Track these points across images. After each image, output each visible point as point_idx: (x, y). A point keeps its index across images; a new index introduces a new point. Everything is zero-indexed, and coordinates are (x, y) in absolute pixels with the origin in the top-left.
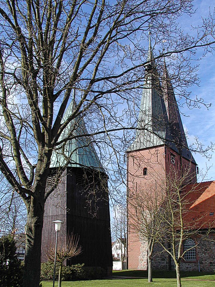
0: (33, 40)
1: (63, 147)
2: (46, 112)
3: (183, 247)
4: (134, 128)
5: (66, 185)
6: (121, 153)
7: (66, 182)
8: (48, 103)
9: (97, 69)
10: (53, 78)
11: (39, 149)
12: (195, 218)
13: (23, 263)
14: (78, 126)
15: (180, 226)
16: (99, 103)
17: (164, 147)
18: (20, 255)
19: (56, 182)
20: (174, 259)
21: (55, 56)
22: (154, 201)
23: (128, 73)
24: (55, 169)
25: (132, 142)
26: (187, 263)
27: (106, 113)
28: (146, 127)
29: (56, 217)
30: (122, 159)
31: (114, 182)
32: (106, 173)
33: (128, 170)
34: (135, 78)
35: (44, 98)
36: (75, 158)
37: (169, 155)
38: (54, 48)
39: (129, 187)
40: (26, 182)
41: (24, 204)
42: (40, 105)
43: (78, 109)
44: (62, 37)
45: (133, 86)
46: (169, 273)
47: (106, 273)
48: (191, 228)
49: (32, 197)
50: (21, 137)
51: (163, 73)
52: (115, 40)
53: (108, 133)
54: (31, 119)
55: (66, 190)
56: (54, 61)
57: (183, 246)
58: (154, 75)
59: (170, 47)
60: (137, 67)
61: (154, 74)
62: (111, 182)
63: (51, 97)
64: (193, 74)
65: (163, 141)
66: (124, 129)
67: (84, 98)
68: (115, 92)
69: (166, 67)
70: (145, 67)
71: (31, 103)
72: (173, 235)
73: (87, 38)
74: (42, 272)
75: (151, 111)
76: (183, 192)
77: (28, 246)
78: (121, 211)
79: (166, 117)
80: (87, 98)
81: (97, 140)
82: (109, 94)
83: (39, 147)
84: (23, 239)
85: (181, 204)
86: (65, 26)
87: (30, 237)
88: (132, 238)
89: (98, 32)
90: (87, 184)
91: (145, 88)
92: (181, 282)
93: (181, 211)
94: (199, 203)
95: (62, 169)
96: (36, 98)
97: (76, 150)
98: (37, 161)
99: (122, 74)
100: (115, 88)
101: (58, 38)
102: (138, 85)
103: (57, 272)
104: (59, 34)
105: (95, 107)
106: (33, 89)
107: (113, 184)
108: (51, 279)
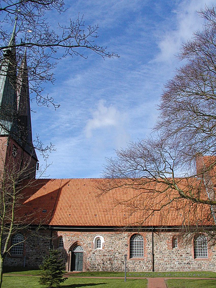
3: (11, 242)
12: (27, 214)
15: (11, 220)
26: (13, 258)
48: (21, 222)
57: (12, 241)
59: (33, 38)
64: (50, 72)
72: (2, 229)
85: (15, 198)
92: (3, 278)
93: (14, 205)
94: (34, 199)
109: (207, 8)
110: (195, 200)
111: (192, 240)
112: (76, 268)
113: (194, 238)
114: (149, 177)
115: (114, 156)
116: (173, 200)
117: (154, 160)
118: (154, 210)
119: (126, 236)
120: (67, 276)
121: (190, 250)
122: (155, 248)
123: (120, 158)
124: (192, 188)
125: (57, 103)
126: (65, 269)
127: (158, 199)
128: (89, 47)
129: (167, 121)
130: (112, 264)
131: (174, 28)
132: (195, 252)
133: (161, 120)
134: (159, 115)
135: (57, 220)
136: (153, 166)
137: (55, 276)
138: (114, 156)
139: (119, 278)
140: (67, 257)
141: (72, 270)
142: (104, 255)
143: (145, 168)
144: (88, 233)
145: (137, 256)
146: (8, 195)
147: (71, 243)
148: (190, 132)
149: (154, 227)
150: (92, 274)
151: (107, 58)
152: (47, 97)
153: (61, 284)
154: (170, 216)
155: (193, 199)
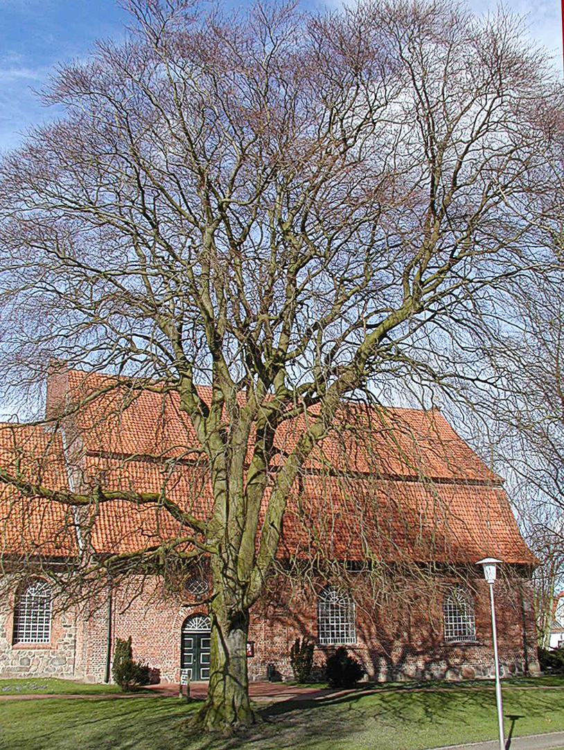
136: (224, 249)
145: (43, 639)
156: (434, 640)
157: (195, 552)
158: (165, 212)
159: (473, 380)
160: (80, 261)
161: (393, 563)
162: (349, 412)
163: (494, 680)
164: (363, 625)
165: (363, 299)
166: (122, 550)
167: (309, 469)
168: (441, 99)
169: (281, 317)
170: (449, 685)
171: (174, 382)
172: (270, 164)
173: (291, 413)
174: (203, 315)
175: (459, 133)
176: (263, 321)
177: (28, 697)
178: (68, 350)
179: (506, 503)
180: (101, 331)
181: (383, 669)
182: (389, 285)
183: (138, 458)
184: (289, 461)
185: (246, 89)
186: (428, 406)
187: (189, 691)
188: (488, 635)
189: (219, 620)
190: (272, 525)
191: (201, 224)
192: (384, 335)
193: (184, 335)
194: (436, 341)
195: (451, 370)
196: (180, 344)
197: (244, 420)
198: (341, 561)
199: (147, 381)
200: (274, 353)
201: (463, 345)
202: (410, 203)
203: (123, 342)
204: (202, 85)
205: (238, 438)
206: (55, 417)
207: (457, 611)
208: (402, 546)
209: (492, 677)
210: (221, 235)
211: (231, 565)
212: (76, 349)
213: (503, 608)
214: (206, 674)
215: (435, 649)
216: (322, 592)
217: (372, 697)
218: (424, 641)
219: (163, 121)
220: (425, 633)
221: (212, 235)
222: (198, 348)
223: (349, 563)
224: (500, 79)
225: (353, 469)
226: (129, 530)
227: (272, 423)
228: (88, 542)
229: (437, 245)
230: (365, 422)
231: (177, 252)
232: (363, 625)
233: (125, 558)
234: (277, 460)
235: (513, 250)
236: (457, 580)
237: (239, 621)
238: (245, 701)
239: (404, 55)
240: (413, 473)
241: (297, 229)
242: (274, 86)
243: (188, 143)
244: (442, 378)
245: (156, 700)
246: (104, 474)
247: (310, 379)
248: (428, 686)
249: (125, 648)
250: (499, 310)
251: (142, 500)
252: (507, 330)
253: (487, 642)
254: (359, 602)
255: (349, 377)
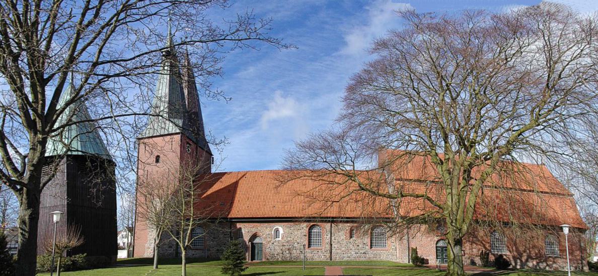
0: (5, 21)
1: (61, 134)
2: (36, 97)
4: (147, 115)
5: (66, 174)
6: (131, 139)
7: (66, 171)
8: (37, 87)
9: (100, 52)
10: (41, 61)
11: (30, 138)
13: (15, 257)
14: (79, 111)
16: (104, 87)
17: (179, 136)
18: (13, 250)
19: (54, 171)
20: (181, 246)
21: (41, 37)
22: (165, 189)
23: (141, 58)
24: (52, 158)
25: (144, 128)
27: (113, 98)
28: (161, 114)
29: (55, 207)
30: (132, 146)
31: (123, 169)
32: (114, 160)
33: (138, 157)
34: (149, 63)
35: (31, 82)
36: (76, 145)
37: (185, 144)
38: (40, 28)
39: (139, 174)
40: (16, 173)
41: (15, 197)
42: (27, 90)
43: (78, 93)
44: (49, 18)
45: (147, 71)
46: (176, 260)
47: (110, 261)
49: (24, 188)
50: (5, 125)
51: (184, 61)
52: (125, 23)
53: (116, 118)
54: (16, 107)
55: (65, 179)
56: (41, 43)
58: (173, 61)
60: (152, 52)
61: (173, 60)
62: (119, 170)
63: (40, 81)
64: (218, 66)
65: (180, 129)
66: (135, 114)
67: (86, 81)
68: (124, 76)
69: (188, 55)
70: (162, 52)
71: (15, 88)
73: (85, 19)
74: (38, 265)
75: (168, 97)
76: (196, 181)
77: (21, 239)
78: (129, 199)
79: (184, 105)
80: (88, 82)
81: (103, 126)
82: (117, 78)
83: (30, 135)
84: (15, 233)
86: (52, 7)
87: (25, 231)
88: (139, 226)
89: (101, 13)
90: (91, 177)
91: (162, 74)
95: (60, 157)
96: (21, 83)
97: (76, 136)
98: (29, 150)
99: (134, 58)
100: (124, 72)
101: (43, 17)
102: (153, 70)
103: (55, 264)
104: (43, 15)
105: (99, 91)
106: (16, 74)
107: (121, 172)
108: (48, 270)
109: (407, 9)
110: (374, 193)
111: (370, 231)
112: (256, 257)
113: (372, 229)
114: (330, 169)
115: (293, 148)
116: (353, 192)
117: (334, 152)
118: (333, 202)
119: (304, 227)
120: (247, 266)
121: (367, 240)
122: (333, 238)
123: (298, 149)
124: (373, 181)
125: (228, 96)
126: (245, 259)
127: (338, 191)
128: (262, 39)
129: (350, 114)
130: (291, 254)
131: (365, 23)
132: (371, 243)
133: (344, 112)
134: (341, 107)
135: (235, 213)
136: (333, 157)
137: (236, 266)
138: (293, 148)
139: (298, 266)
140: (246, 248)
141: (252, 260)
142: (283, 246)
143: (325, 160)
144: (266, 224)
146: (186, 191)
147: (251, 235)
148: (374, 126)
149: (333, 218)
150: (272, 263)
151: (284, 50)
152: (217, 91)
153: (242, 273)
154: (348, 208)
155: (372, 192)
156: (540, 254)
157: (440, 216)
158: (422, 88)
159: (561, 154)
160: (388, 109)
161: (522, 223)
162: (504, 164)
163: (568, 272)
164: (510, 247)
165: (511, 120)
166: (411, 215)
167: (486, 186)
168: (557, 44)
169: (474, 126)
170: (547, 272)
171: (428, 152)
172: (470, 69)
173: (478, 164)
174: (440, 126)
175: (565, 58)
176: (466, 128)
177: (381, 267)
178: (386, 142)
179: (574, 205)
180: (398, 134)
181: (519, 264)
182: (524, 115)
183: (415, 181)
184: (477, 182)
185: (459, 41)
186: (540, 163)
187: (440, 267)
188: (564, 257)
189: (450, 242)
190: (471, 206)
191: (438, 92)
192: (520, 134)
193: (432, 134)
194: (545, 138)
195: (551, 149)
196: (430, 137)
197: (458, 166)
198: (500, 222)
199: (417, 152)
200: (470, 140)
201: (557, 140)
202: (536, 84)
203: (407, 138)
204: (438, 41)
205: (456, 173)
206: (382, 167)
207: (551, 244)
208: (527, 217)
209: (567, 270)
210: (447, 95)
211: (454, 221)
212: (388, 141)
213: (572, 244)
214: (446, 261)
215: (540, 257)
216: (492, 233)
217: (514, 274)
218: (536, 254)
219: (421, 55)
220: (537, 251)
221: (443, 96)
222: (438, 139)
223: (503, 222)
224: (591, 38)
225: (505, 186)
226: (414, 207)
227: (470, 167)
228: (398, 212)
229: (548, 100)
230: (510, 168)
231: (428, 103)
232: (510, 247)
233: (412, 218)
234: (472, 182)
235: (586, 104)
236: (551, 232)
237: (458, 242)
238: (462, 272)
239: (540, 27)
240: (532, 189)
241: (482, 93)
242: (473, 40)
243: (432, 62)
244: (547, 152)
245: (428, 270)
246: (402, 187)
247: (486, 151)
248: (538, 272)
249: (415, 251)
250: (576, 127)
251: (418, 196)
252: (579, 135)
253: (564, 257)
254: (508, 237)
255: (504, 150)
